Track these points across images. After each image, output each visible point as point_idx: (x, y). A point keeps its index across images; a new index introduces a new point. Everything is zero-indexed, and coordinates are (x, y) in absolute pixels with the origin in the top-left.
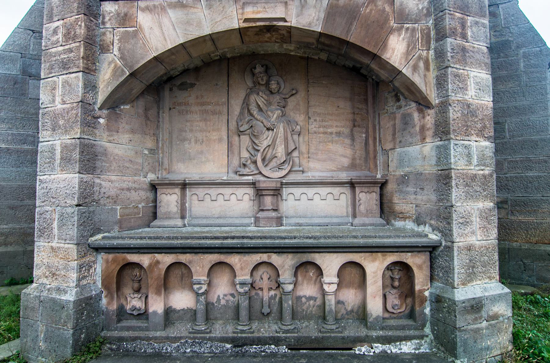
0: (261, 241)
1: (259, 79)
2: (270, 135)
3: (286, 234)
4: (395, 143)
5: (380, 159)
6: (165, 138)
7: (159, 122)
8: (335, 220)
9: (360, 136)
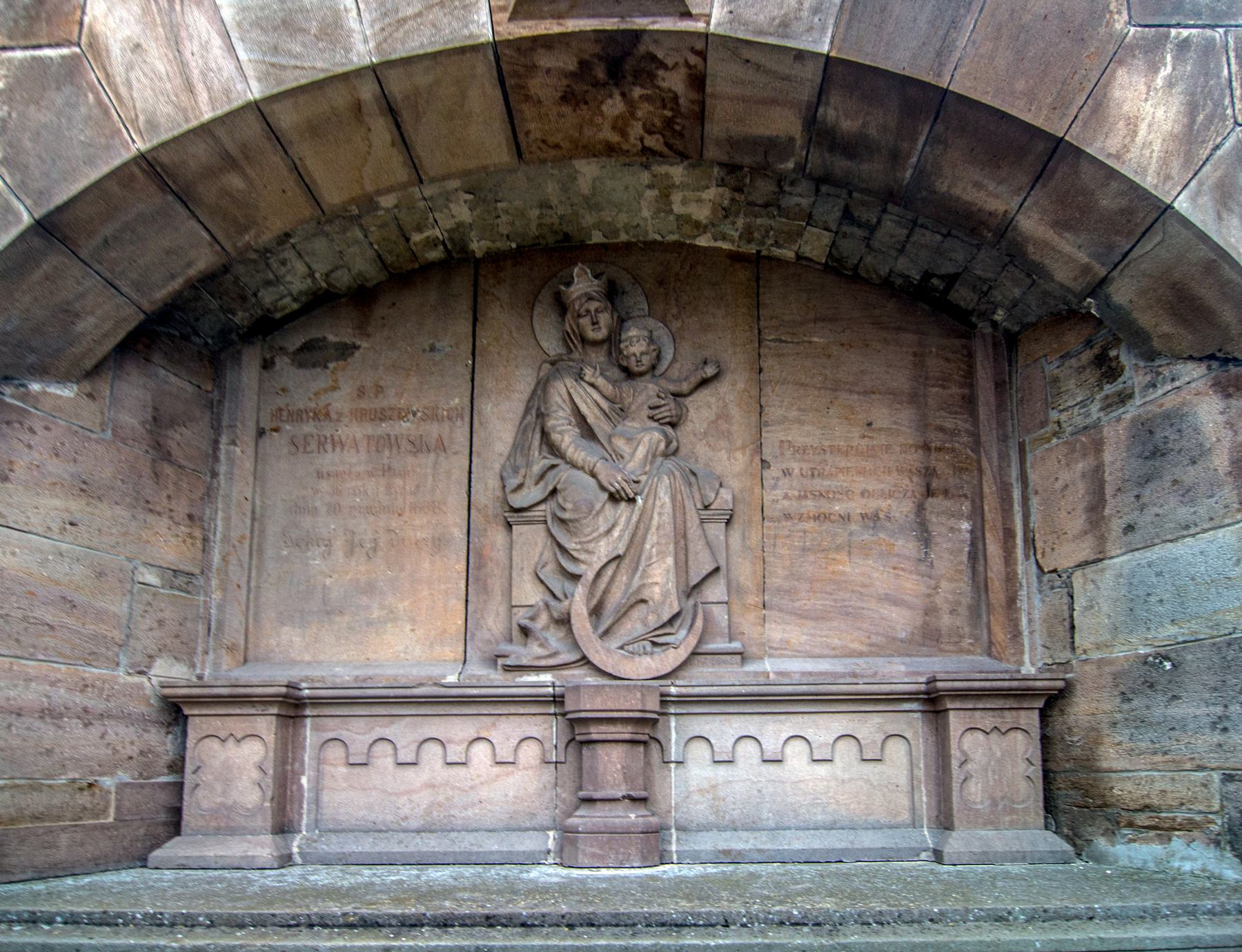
0: (569, 942)
1: (585, 321)
2: (623, 520)
3: (685, 905)
4: (1102, 539)
5: (1034, 606)
6: (234, 534)
7: (214, 474)
8: (869, 840)
9: (952, 529)
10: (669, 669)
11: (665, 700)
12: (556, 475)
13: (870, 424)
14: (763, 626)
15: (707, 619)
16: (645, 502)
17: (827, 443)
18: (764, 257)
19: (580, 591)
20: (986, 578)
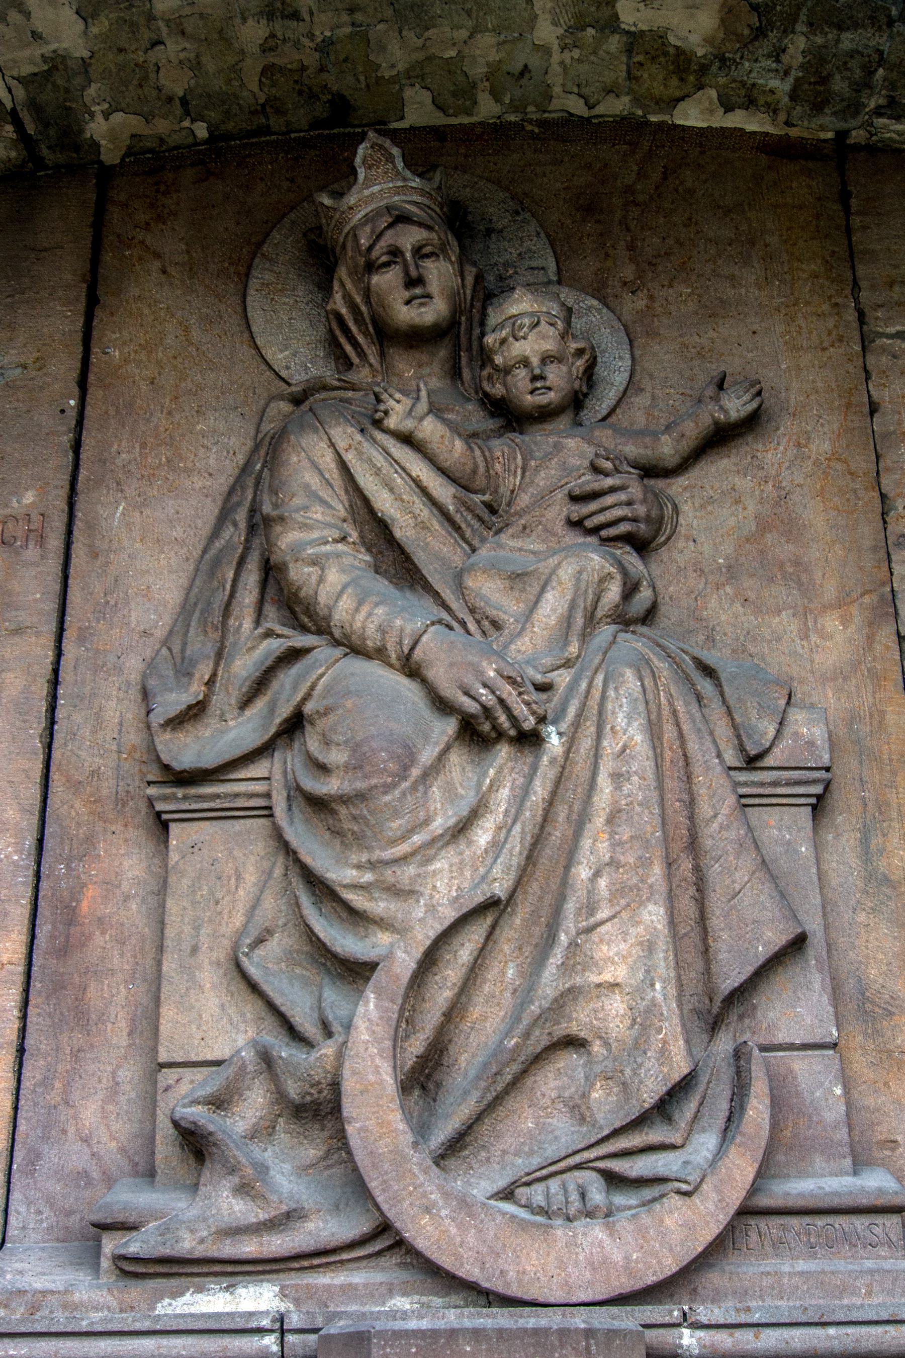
1: (388, 281)
10: (670, 1266)
12: (300, 678)
15: (780, 1103)
18: (857, 148)
19: (369, 1015)
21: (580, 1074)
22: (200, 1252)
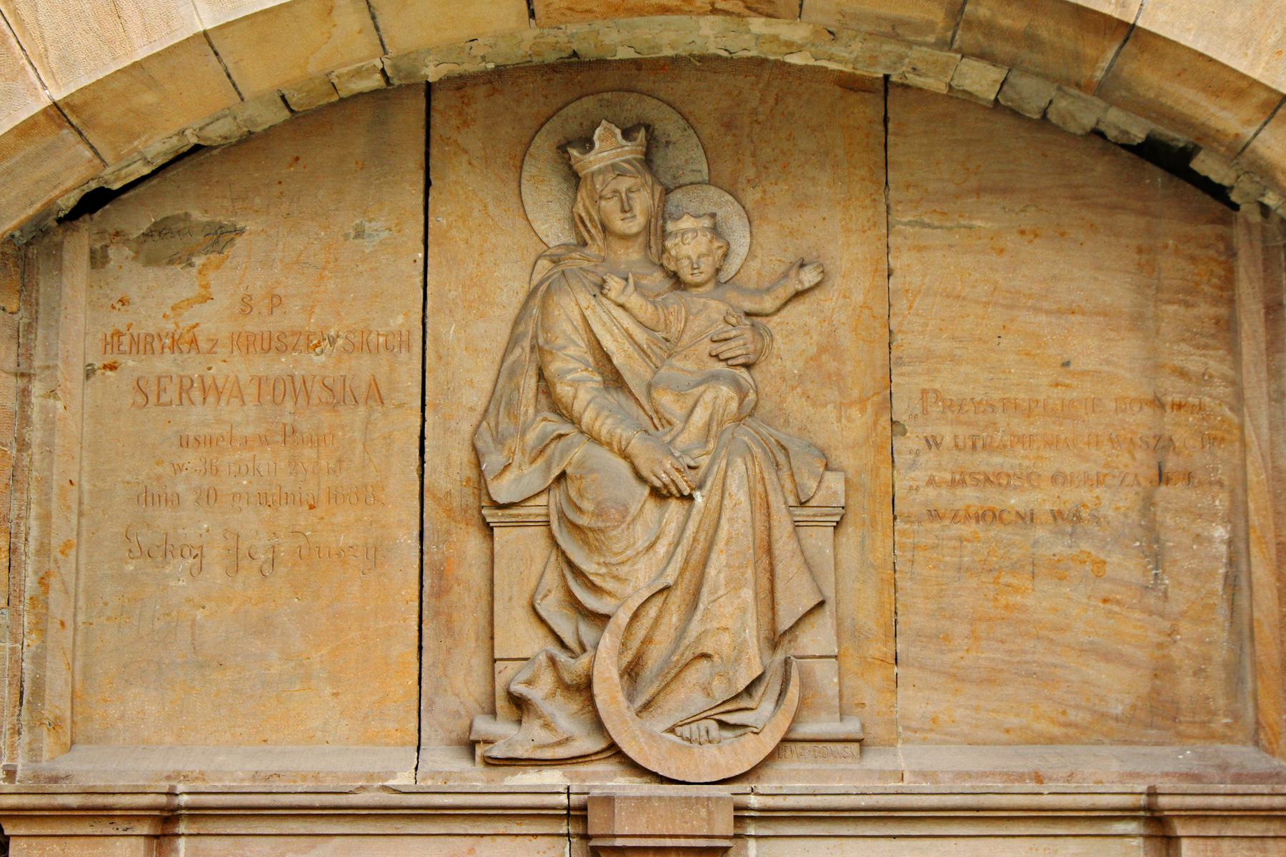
1: (611, 206)
10: (747, 768)
11: (741, 815)
13: (1066, 364)
14: (895, 692)
16: (708, 499)
17: (996, 395)
19: (608, 642)
20: (1251, 620)
21: (707, 671)
22: (526, 756)
